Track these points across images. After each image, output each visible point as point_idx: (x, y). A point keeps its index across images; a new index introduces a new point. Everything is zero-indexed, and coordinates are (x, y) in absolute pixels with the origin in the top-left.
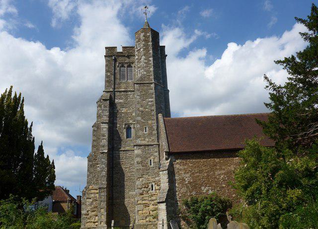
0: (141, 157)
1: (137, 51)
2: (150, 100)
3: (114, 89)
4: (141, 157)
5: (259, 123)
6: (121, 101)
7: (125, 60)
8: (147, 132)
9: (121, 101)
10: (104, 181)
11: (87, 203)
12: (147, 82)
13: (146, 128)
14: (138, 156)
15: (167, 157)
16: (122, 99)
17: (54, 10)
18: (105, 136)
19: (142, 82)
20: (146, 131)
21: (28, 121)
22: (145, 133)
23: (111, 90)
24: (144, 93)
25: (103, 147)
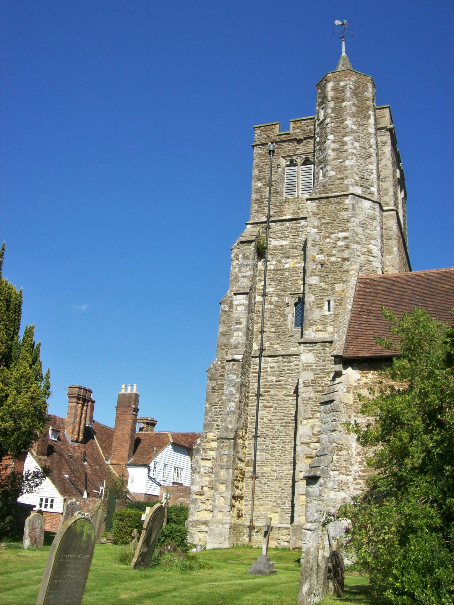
0: (313, 370)
1: (319, 125)
2: (342, 235)
3: (269, 216)
4: (313, 370)
5: (8, 301)
6: (284, 243)
7: (297, 149)
8: (331, 312)
9: (284, 243)
10: (231, 423)
11: (202, 470)
12: (337, 194)
13: (329, 302)
14: (307, 367)
15: (388, 371)
16: (286, 238)
17: (322, 582)
18: (241, 323)
19: (324, 195)
20: (329, 310)
21: (37, 339)
22: (327, 313)
23: (264, 219)
24: (327, 220)
25: (236, 347)
